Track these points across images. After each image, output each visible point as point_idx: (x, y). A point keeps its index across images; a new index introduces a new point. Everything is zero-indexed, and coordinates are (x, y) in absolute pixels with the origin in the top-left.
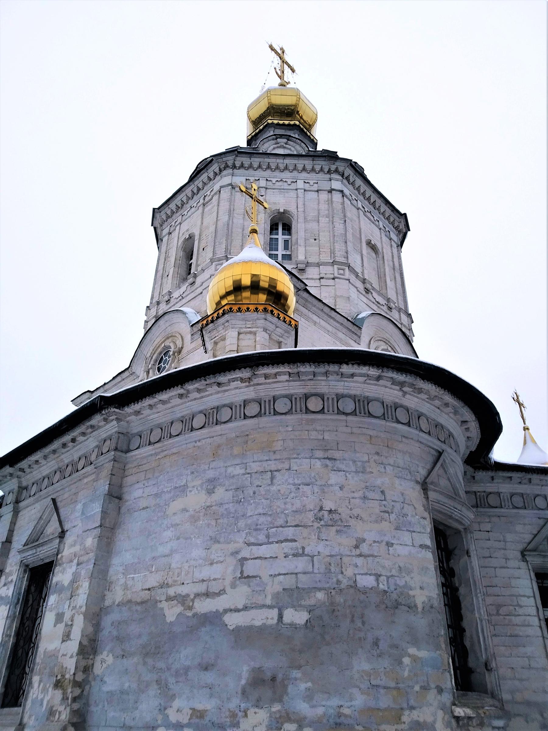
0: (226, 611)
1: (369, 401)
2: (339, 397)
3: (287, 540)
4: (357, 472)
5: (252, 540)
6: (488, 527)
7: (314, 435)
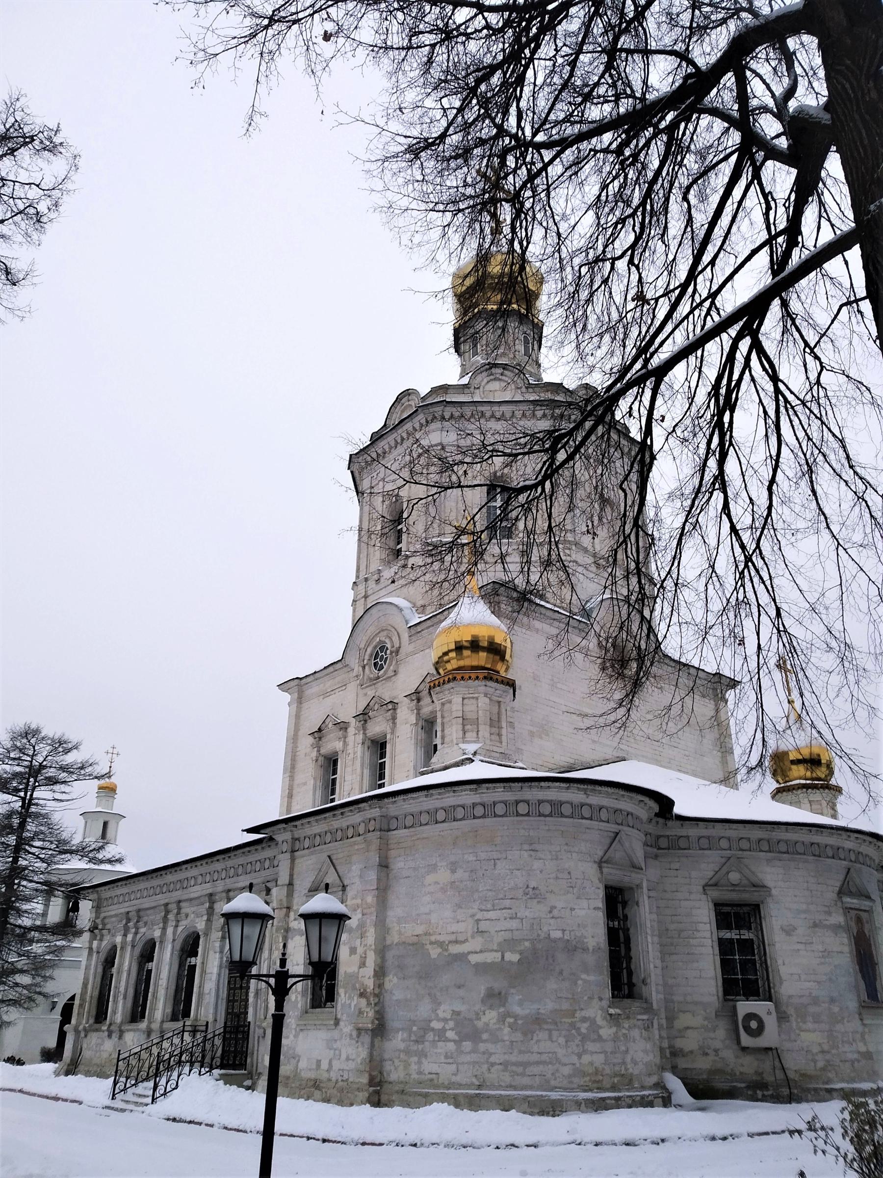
0: (469, 953)
1: (561, 803)
2: (540, 802)
3: (505, 908)
4: (552, 859)
5: (483, 908)
6: (677, 866)
7: (522, 832)
